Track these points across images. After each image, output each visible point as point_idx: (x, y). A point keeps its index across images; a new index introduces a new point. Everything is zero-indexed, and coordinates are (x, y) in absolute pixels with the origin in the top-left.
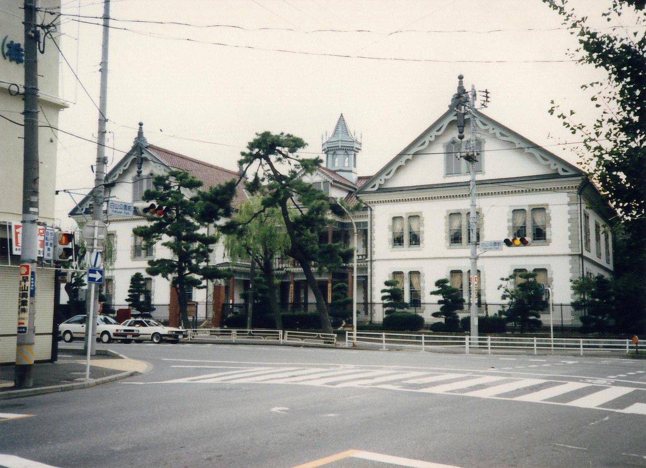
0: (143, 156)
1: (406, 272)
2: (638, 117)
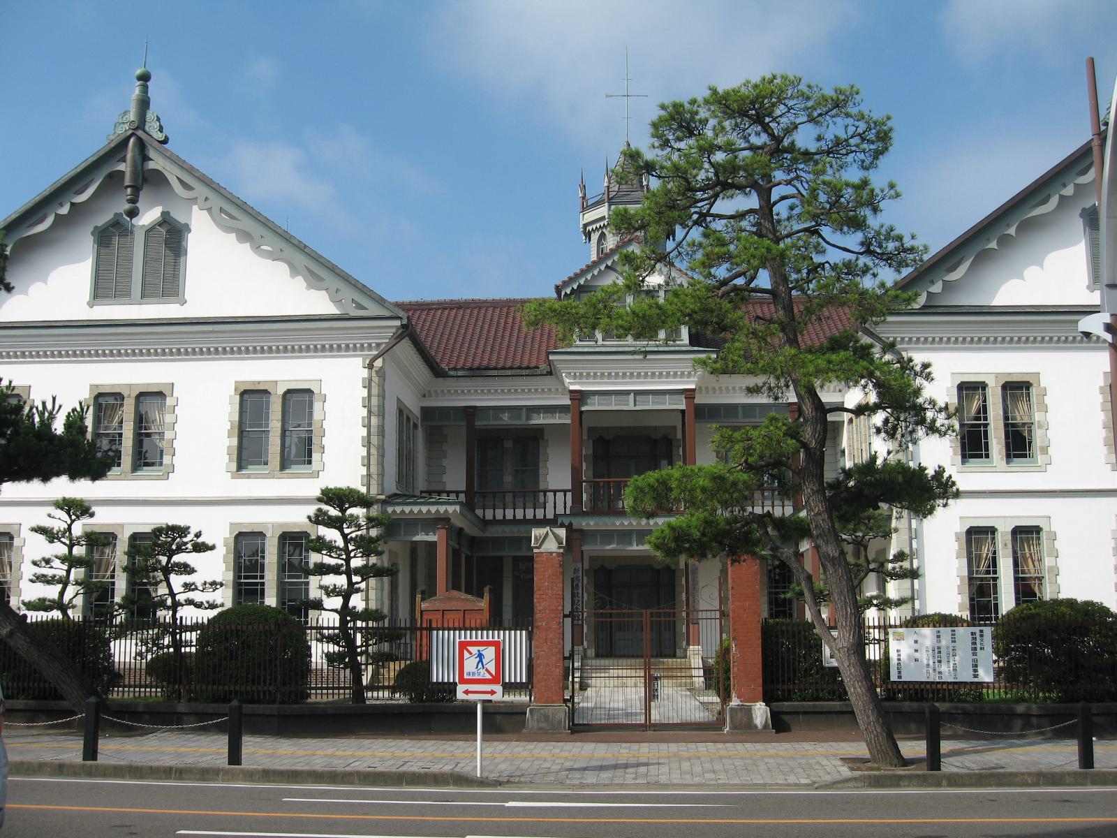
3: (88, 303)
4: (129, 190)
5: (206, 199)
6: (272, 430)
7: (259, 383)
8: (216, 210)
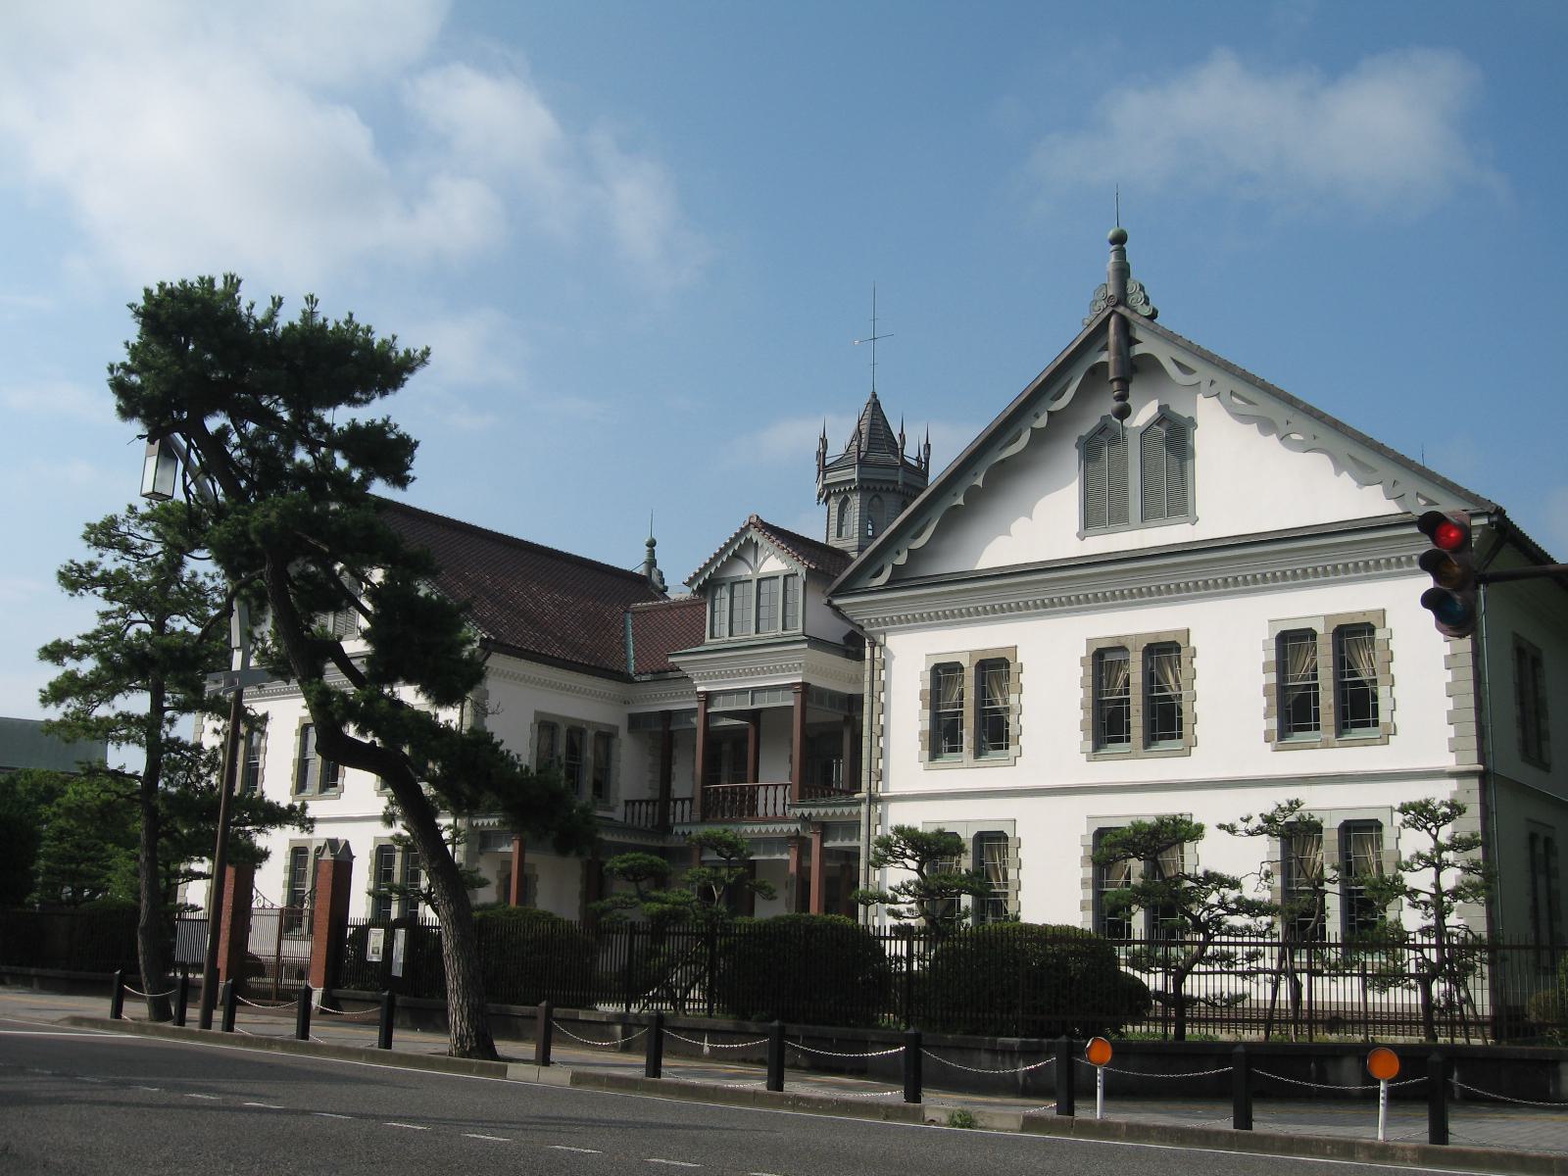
0: (1138, 350)
1: (1331, 824)
2: (369, 492)
3: (1078, 535)
4: (1115, 385)
5: (1212, 382)
6: (1327, 689)
7: (1364, 614)
8: (1225, 394)
